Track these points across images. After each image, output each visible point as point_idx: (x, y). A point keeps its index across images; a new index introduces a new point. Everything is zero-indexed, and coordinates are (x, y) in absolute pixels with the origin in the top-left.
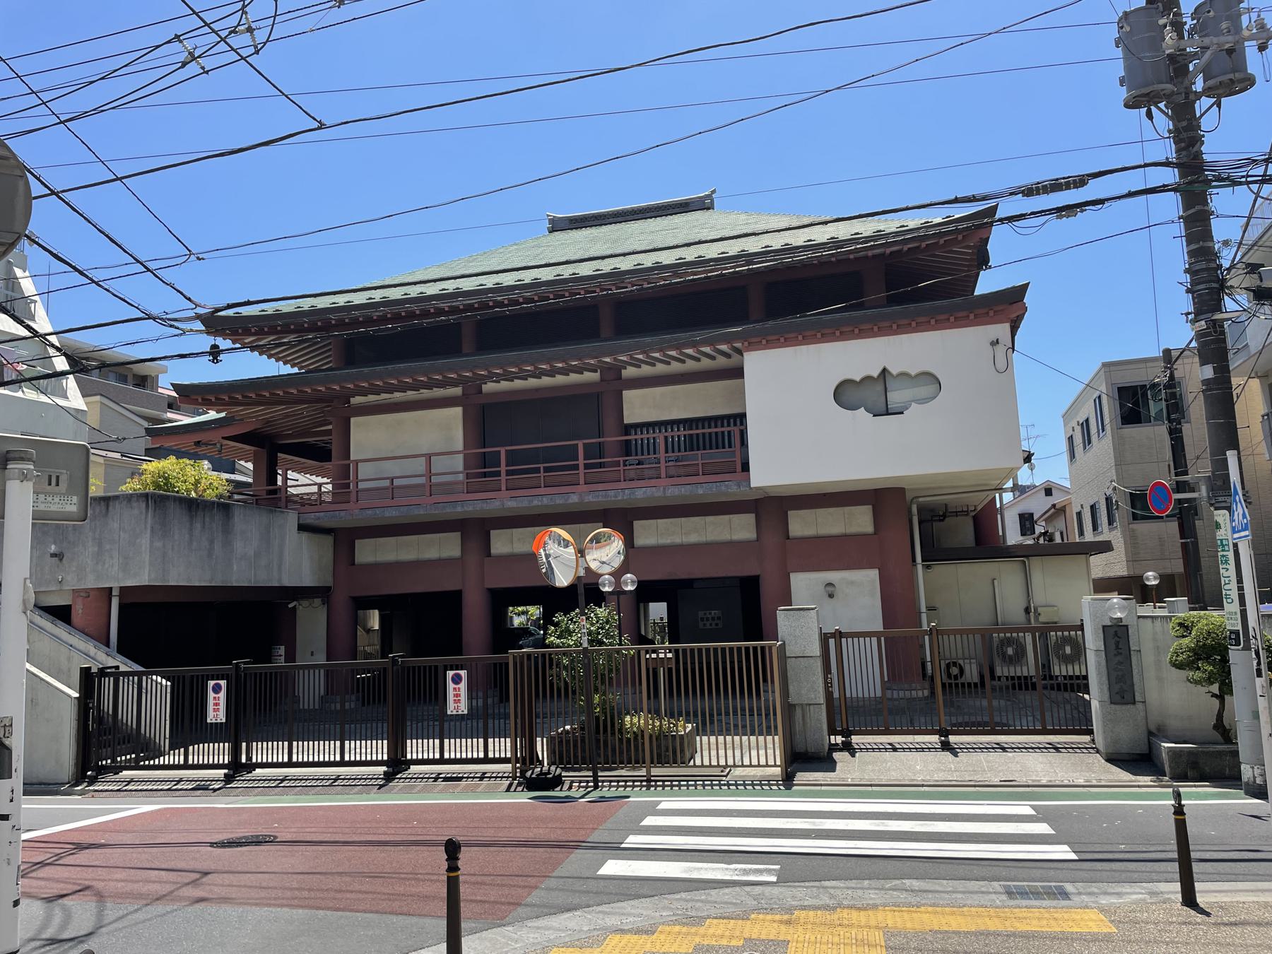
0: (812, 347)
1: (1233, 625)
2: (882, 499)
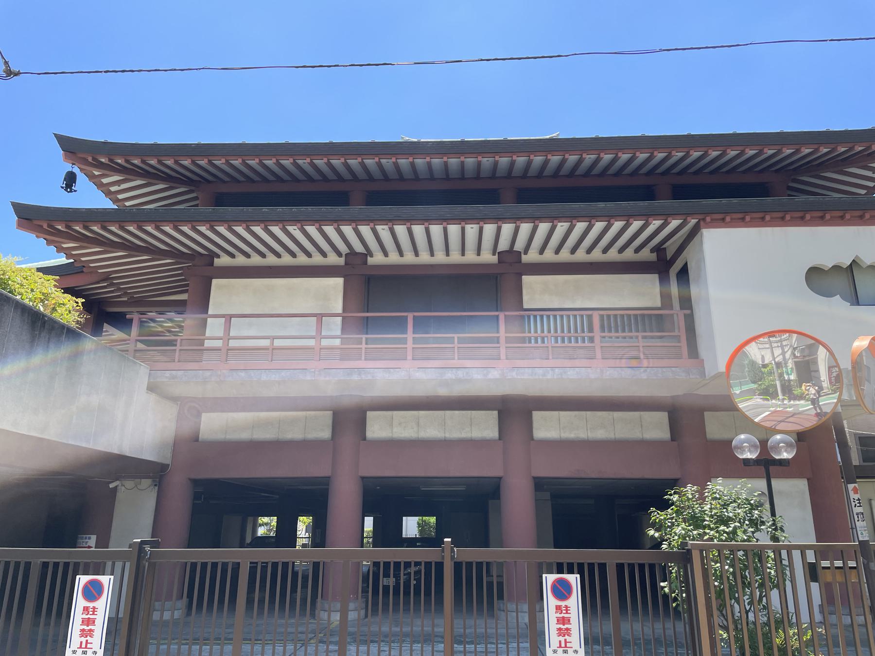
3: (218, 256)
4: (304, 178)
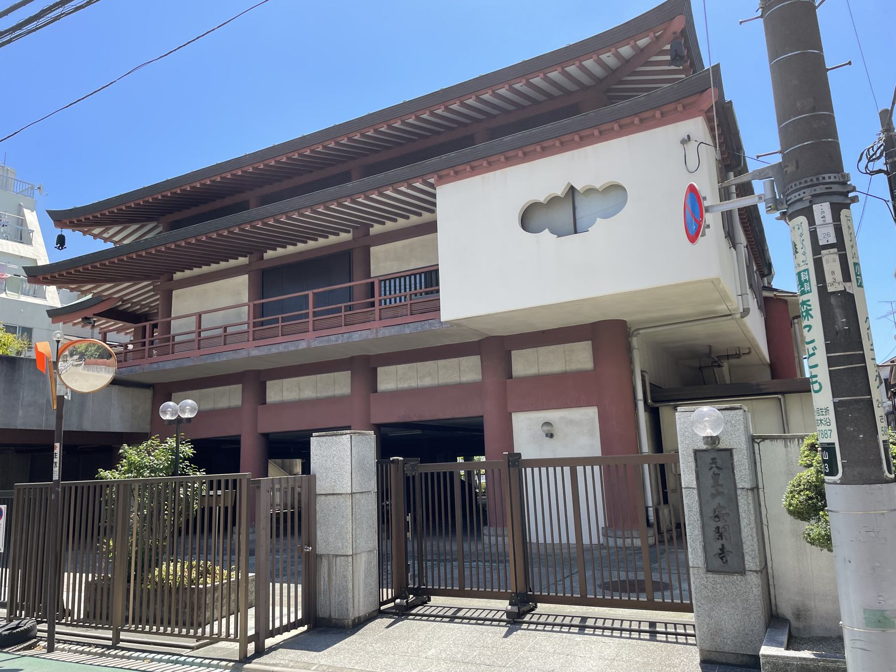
0: (498, 173)
1: (825, 434)
2: (608, 335)
3: (372, 226)
4: (543, 98)
